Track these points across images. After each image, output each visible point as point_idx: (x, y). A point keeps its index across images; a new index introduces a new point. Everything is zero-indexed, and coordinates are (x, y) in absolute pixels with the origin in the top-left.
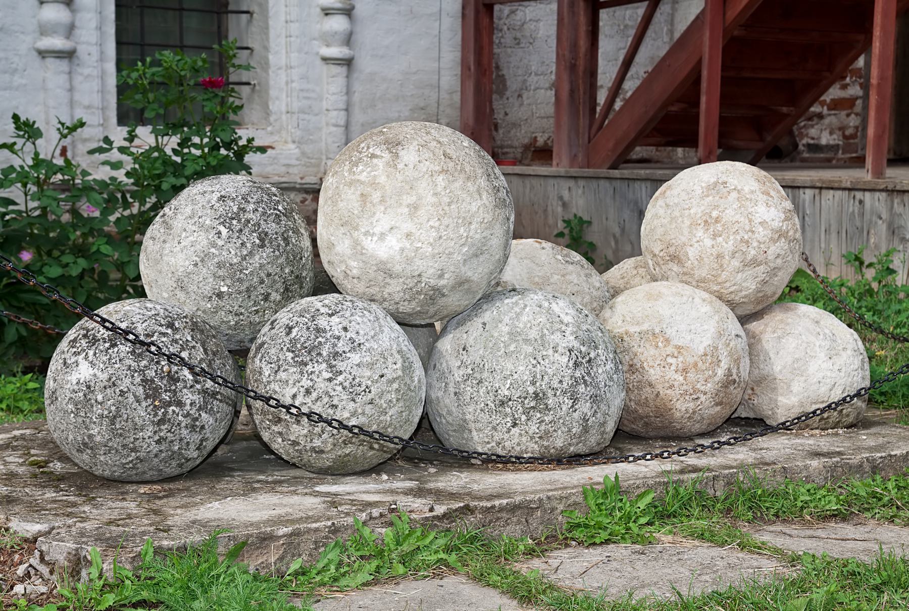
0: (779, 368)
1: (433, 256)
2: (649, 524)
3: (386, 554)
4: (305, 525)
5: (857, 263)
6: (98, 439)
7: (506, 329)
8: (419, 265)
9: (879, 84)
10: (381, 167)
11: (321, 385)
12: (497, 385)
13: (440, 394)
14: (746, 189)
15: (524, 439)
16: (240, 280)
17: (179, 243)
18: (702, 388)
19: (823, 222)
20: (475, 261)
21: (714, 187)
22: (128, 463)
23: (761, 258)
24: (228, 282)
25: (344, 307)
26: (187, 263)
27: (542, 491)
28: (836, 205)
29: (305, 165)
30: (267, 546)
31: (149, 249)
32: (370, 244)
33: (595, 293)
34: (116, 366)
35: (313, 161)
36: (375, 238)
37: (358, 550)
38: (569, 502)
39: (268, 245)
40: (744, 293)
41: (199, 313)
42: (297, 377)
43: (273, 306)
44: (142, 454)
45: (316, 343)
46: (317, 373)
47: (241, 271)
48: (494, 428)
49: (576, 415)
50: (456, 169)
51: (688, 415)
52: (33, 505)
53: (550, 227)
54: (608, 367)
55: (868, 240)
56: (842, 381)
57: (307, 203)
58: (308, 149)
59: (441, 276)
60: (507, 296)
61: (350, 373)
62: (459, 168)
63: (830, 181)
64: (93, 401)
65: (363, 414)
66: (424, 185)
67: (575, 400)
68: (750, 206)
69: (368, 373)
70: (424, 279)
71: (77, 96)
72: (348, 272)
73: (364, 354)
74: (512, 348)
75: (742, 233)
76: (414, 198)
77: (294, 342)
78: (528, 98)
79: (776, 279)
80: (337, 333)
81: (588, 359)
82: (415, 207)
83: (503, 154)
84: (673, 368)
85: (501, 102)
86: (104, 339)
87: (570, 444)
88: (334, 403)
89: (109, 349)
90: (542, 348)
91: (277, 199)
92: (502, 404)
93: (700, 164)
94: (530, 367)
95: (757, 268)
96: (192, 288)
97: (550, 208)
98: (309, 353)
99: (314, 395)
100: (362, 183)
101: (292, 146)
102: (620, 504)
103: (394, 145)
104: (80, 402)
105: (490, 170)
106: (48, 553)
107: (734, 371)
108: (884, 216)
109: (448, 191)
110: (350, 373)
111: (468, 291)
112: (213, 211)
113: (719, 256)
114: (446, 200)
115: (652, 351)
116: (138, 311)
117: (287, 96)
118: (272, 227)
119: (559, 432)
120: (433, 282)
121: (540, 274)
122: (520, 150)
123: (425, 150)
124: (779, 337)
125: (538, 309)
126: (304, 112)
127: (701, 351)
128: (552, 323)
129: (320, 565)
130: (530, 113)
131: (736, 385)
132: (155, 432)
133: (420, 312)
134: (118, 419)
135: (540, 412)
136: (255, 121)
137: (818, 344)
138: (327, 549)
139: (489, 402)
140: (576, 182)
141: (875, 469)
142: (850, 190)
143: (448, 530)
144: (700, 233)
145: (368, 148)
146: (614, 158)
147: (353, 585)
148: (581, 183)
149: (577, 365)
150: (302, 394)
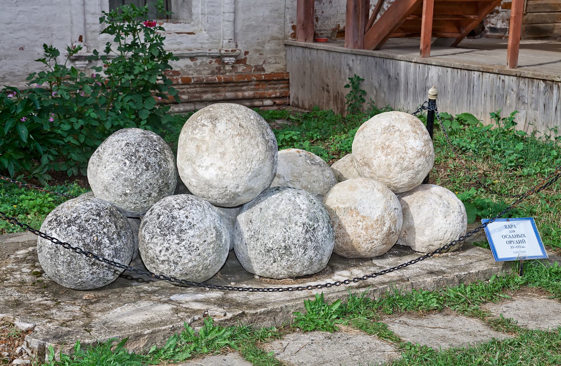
0: (419, 222)
1: (233, 178)
2: (338, 318)
3: (200, 340)
4: (159, 328)
5: (497, 118)
6: (62, 272)
7: (272, 212)
8: (226, 183)
9: (515, 16)
10: (207, 132)
11: (174, 246)
12: (266, 242)
13: (239, 243)
14: (404, 130)
15: (280, 268)
16: (136, 187)
17: (105, 168)
18: (375, 237)
19: (483, 90)
20: (255, 179)
21: (389, 129)
22: (78, 284)
23: (411, 166)
24: (130, 188)
25: (187, 204)
26: (109, 178)
27: (283, 301)
28: (490, 81)
29: (211, 43)
30: (139, 339)
31: (91, 169)
32: (201, 172)
33: (326, 180)
34: (70, 237)
35: (216, 41)
36: (203, 169)
37: (186, 339)
38: (297, 308)
39: (150, 169)
40: (402, 183)
41: (116, 202)
42: (162, 241)
43: (154, 199)
44: (84, 280)
45: (172, 225)
46: (172, 240)
47: (136, 183)
48: (265, 263)
49: (306, 257)
50: (245, 133)
51: (368, 250)
52: (29, 307)
53: (342, 80)
54: (324, 231)
55: (506, 102)
56: (451, 229)
57: (212, 63)
58: (213, 34)
59: (237, 187)
60: (274, 193)
61: (189, 241)
62: (247, 133)
63: (487, 69)
64: (59, 254)
65: (195, 260)
66: (228, 142)
67: (306, 249)
68: (406, 139)
69: (198, 240)
70: (228, 189)
71: (87, 8)
72: (191, 183)
73: (196, 230)
74: (274, 223)
75: (401, 154)
76: (223, 149)
77: (161, 223)
78: (335, 3)
79: (419, 176)
80: (182, 219)
81: (313, 228)
82: (223, 154)
83: (321, 34)
84: (360, 227)
85: (320, 6)
86: (64, 222)
87: (303, 271)
88: (180, 255)
89: (67, 228)
90: (289, 223)
91: (156, 143)
92: (268, 251)
93: (452, 2)
94: (283, 233)
95: (408, 171)
96: (112, 191)
97: (342, 70)
98: (168, 229)
99: (170, 251)
100: (198, 140)
101: (204, 32)
102: (323, 308)
103: (214, 119)
104: (53, 254)
105: (264, 131)
106: (30, 344)
107: (393, 228)
108: (515, 90)
109: (240, 145)
110: (189, 241)
111: (253, 193)
112: (122, 151)
113: (389, 165)
114: (240, 150)
115: (350, 218)
116: (82, 207)
117: (202, 5)
118: (152, 160)
119: (298, 265)
120: (233, 190)
121: (297, 171)
122: (330, 32)
123: (230, 123)
124: (420, 206)
125: (289, 201)
126: (211, 14)
127: (375, 218)
128: (295, 209)
129: (166, 348)
130: (336, 11)
131: (394, 234)
132: (90, 270)
133: (228, 203)
134: (72, 264)
135: (288, 256)
136: (185, 18)
137: (439, 210)
138: (170, 339)
139: (262, 250)
140: (356, 57)
141: (461, 281)
142: (497, 74)
143: (233, 326)
144: (379, 153)
145: (202, 120)
146: (378, 44)
147: (181, 359)
148: (359, 57)
149: (307, 232)
150: (164, 250)
